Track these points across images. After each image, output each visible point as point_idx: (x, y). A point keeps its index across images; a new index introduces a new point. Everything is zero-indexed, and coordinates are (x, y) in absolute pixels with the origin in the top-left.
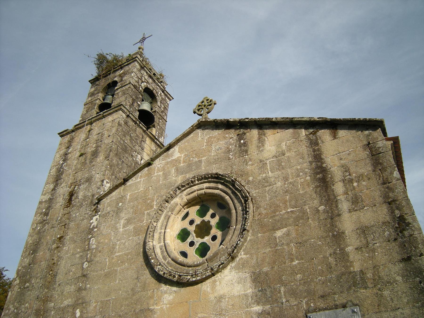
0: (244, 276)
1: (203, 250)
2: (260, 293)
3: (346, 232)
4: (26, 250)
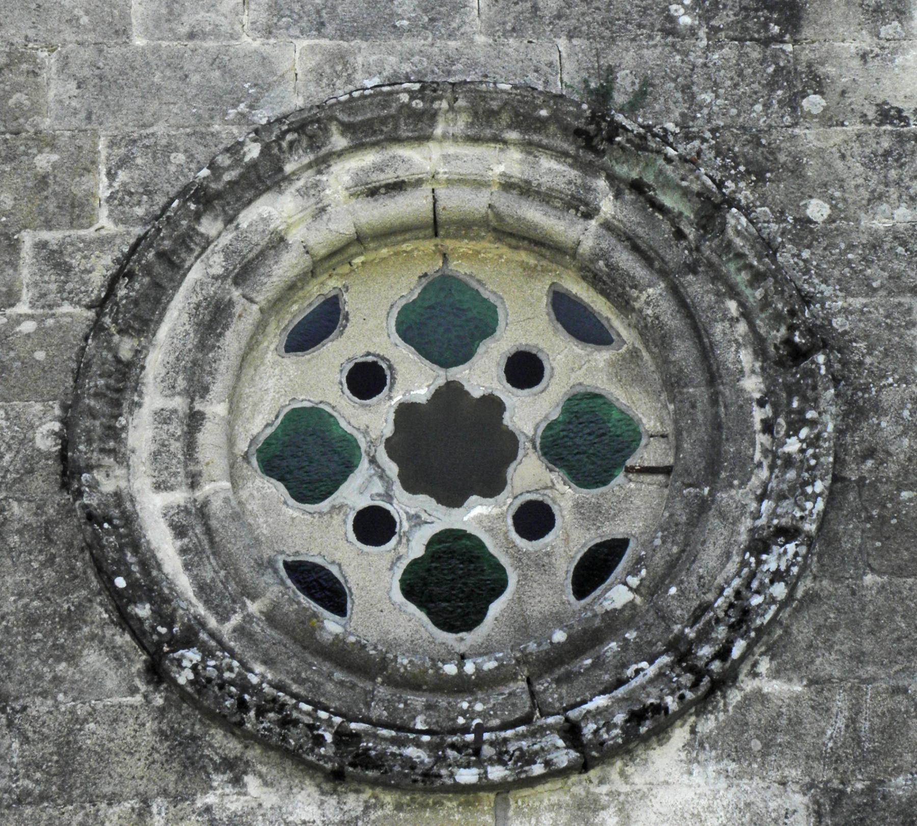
0: (772, 805)
1: (453, 583)
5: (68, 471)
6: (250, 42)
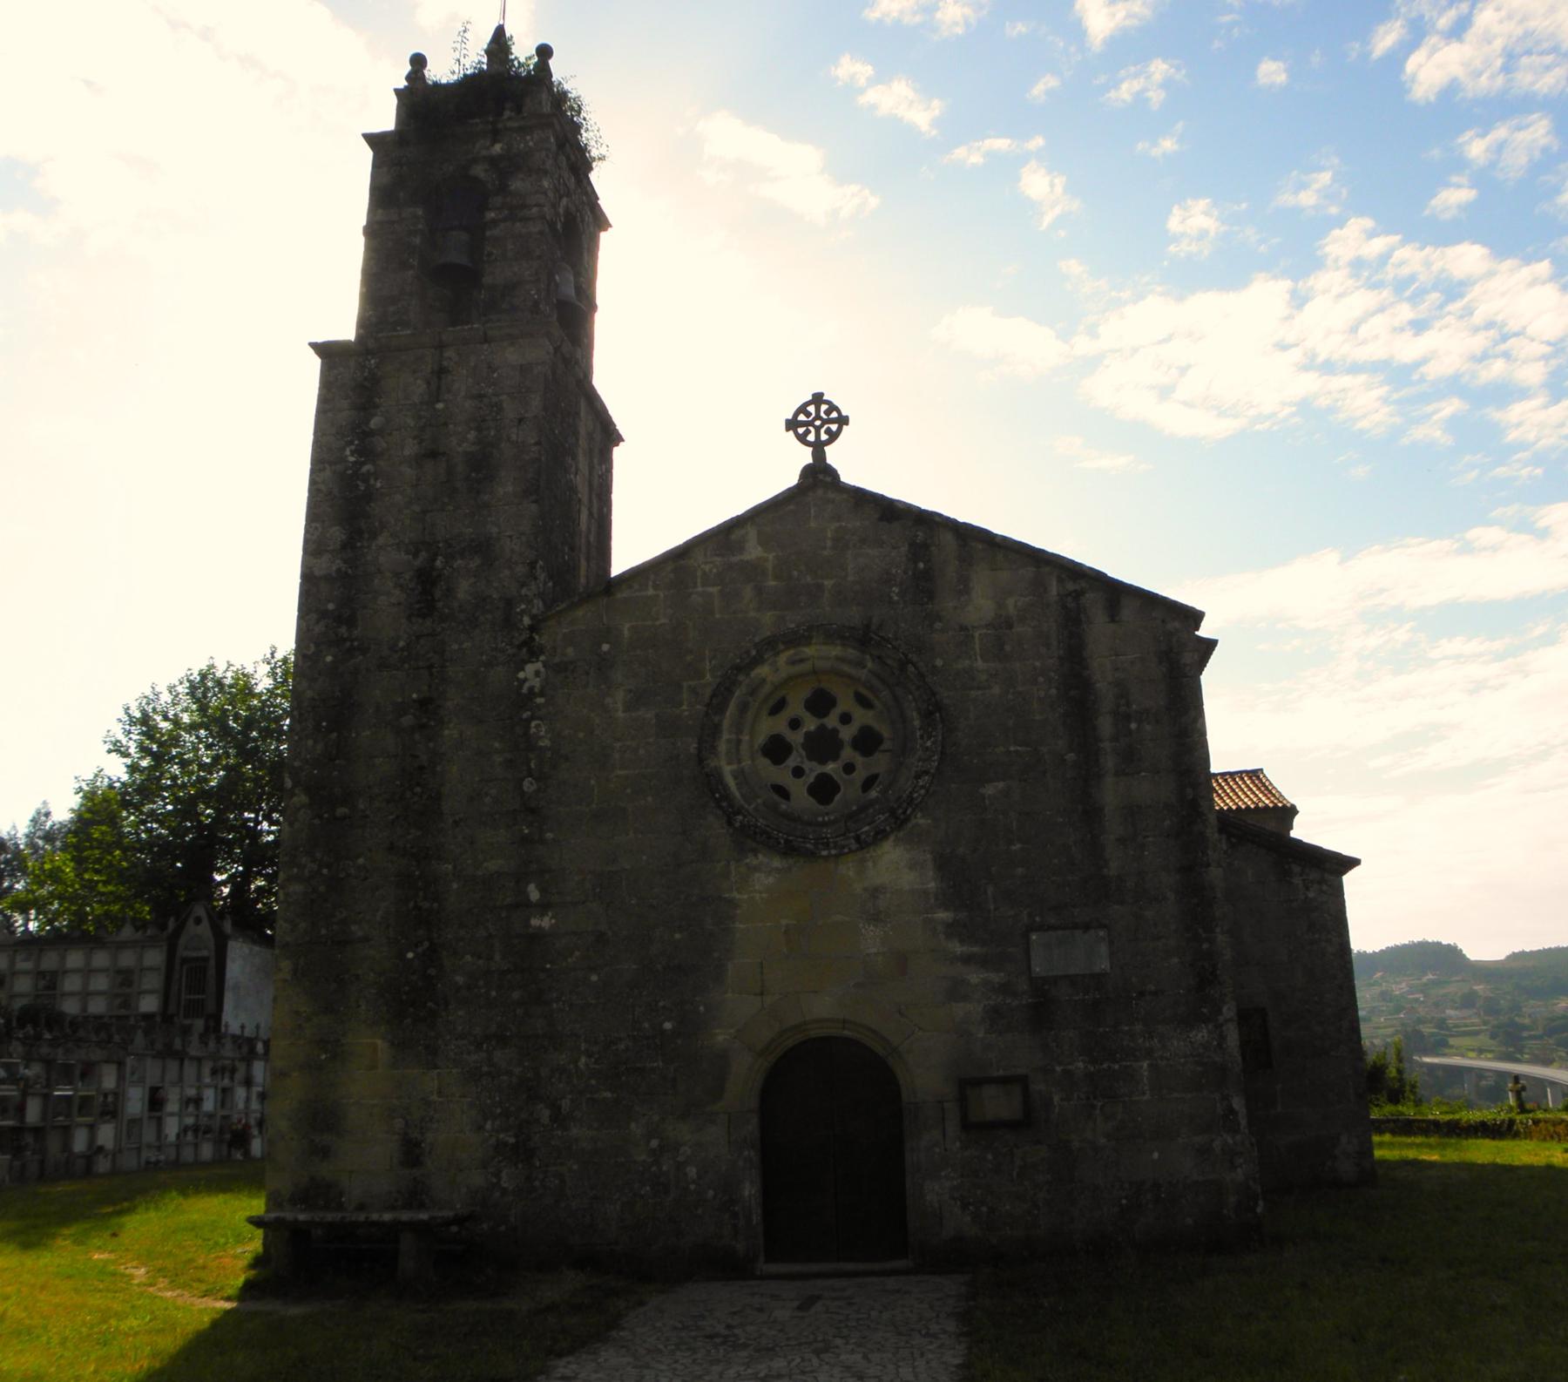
1: (824, 789)
5: (701, 761)
6: (752, 614)
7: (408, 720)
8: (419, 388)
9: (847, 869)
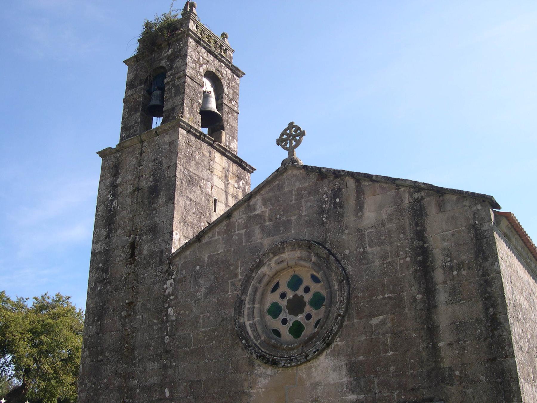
2: (355, 382)
3: (441, 326)
4: (89, 315)
7: (124, 314)
8: (134, 161)
9: (302, 371)
